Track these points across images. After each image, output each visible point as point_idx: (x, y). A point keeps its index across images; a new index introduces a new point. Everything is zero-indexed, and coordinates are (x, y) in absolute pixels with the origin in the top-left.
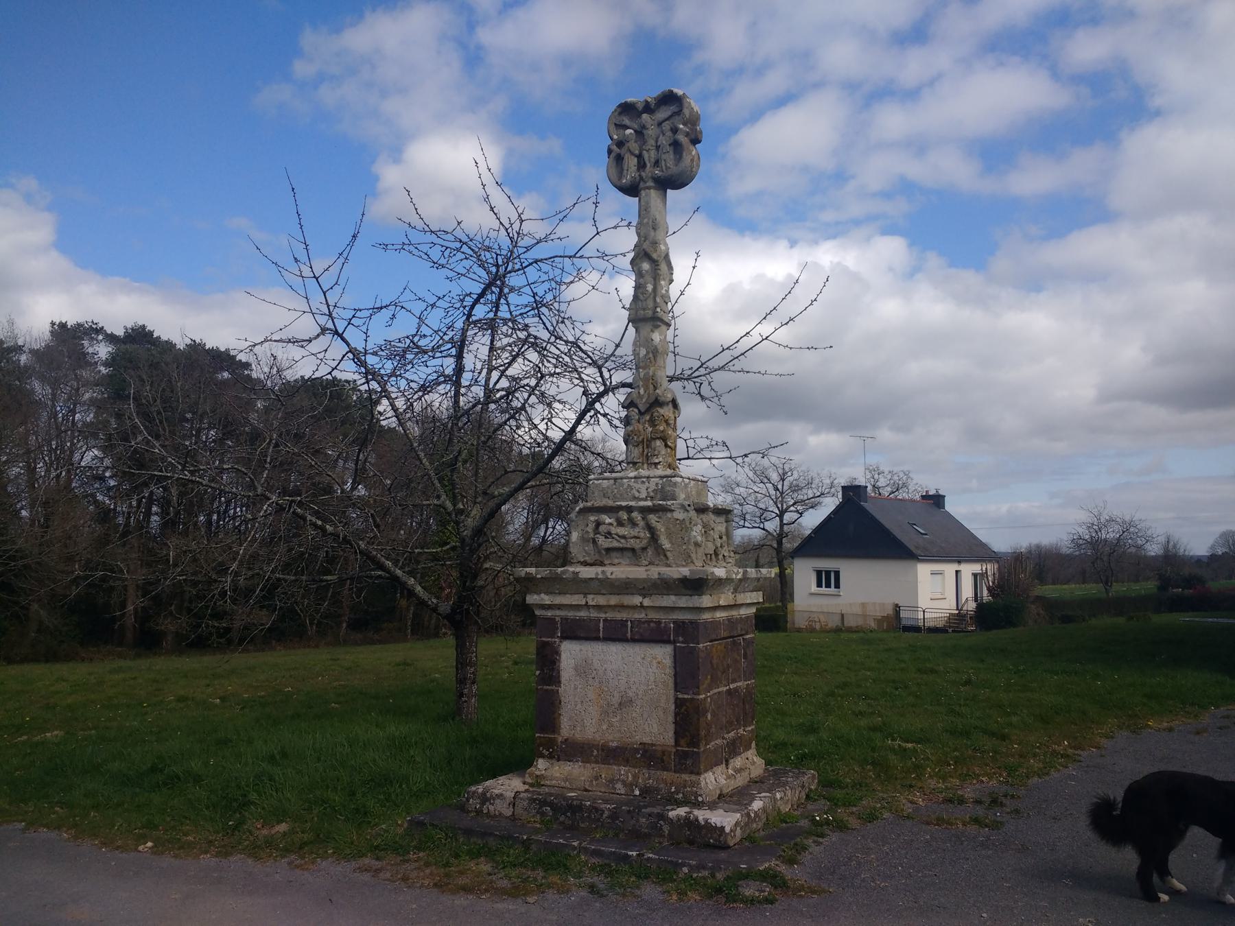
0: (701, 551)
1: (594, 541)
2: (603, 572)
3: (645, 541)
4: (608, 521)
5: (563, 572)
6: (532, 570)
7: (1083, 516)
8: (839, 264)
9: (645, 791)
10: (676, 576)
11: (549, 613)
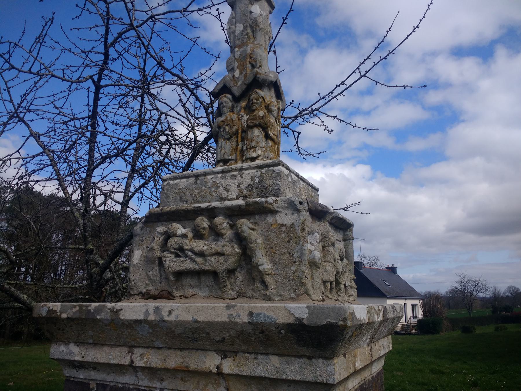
0: (319, 275)
1: (161, 263)
2: (157, 310)
3: (232, 260)
4: (181, 230)
5: (98, 310)
6: (56, 306)
7: (459, 279)
8: (341, 174)
10: (282, 319)
11: (81, 375)
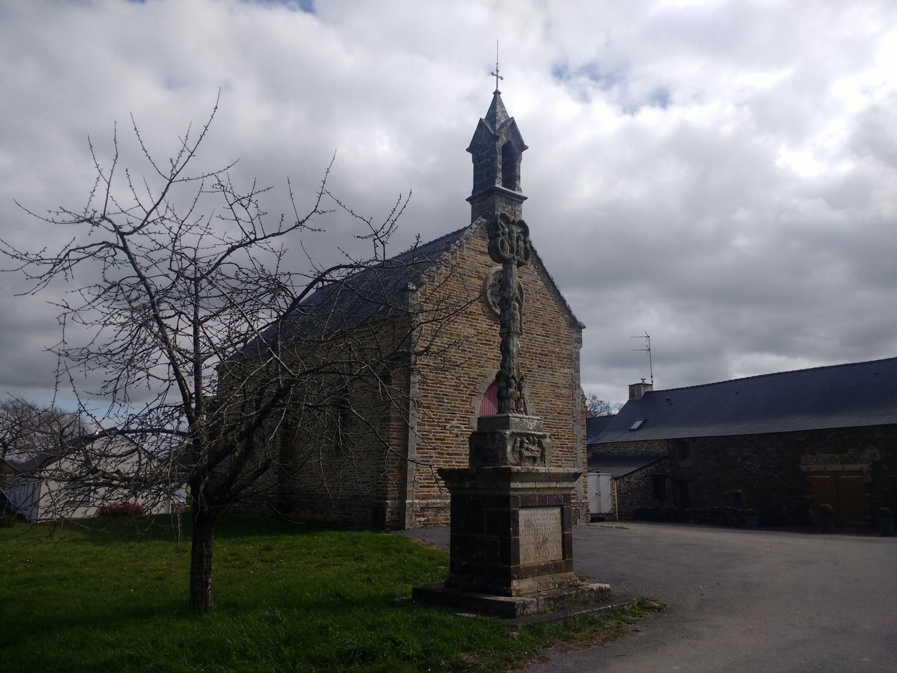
9: (560, 585)
11: (516, 493)
